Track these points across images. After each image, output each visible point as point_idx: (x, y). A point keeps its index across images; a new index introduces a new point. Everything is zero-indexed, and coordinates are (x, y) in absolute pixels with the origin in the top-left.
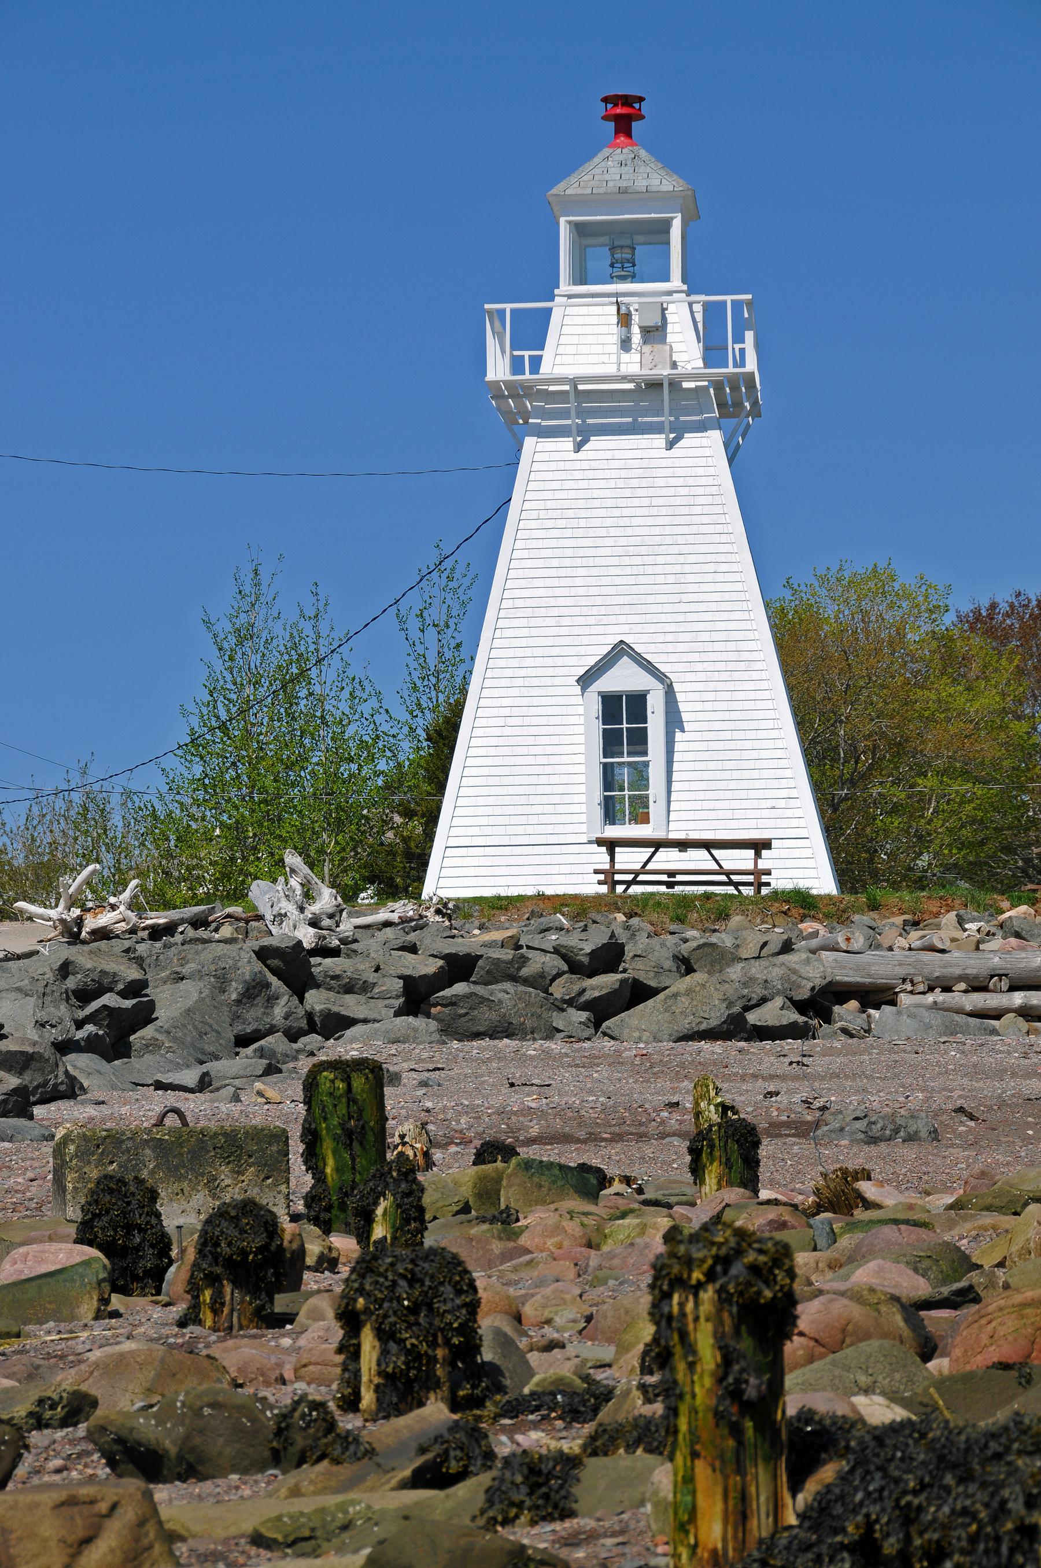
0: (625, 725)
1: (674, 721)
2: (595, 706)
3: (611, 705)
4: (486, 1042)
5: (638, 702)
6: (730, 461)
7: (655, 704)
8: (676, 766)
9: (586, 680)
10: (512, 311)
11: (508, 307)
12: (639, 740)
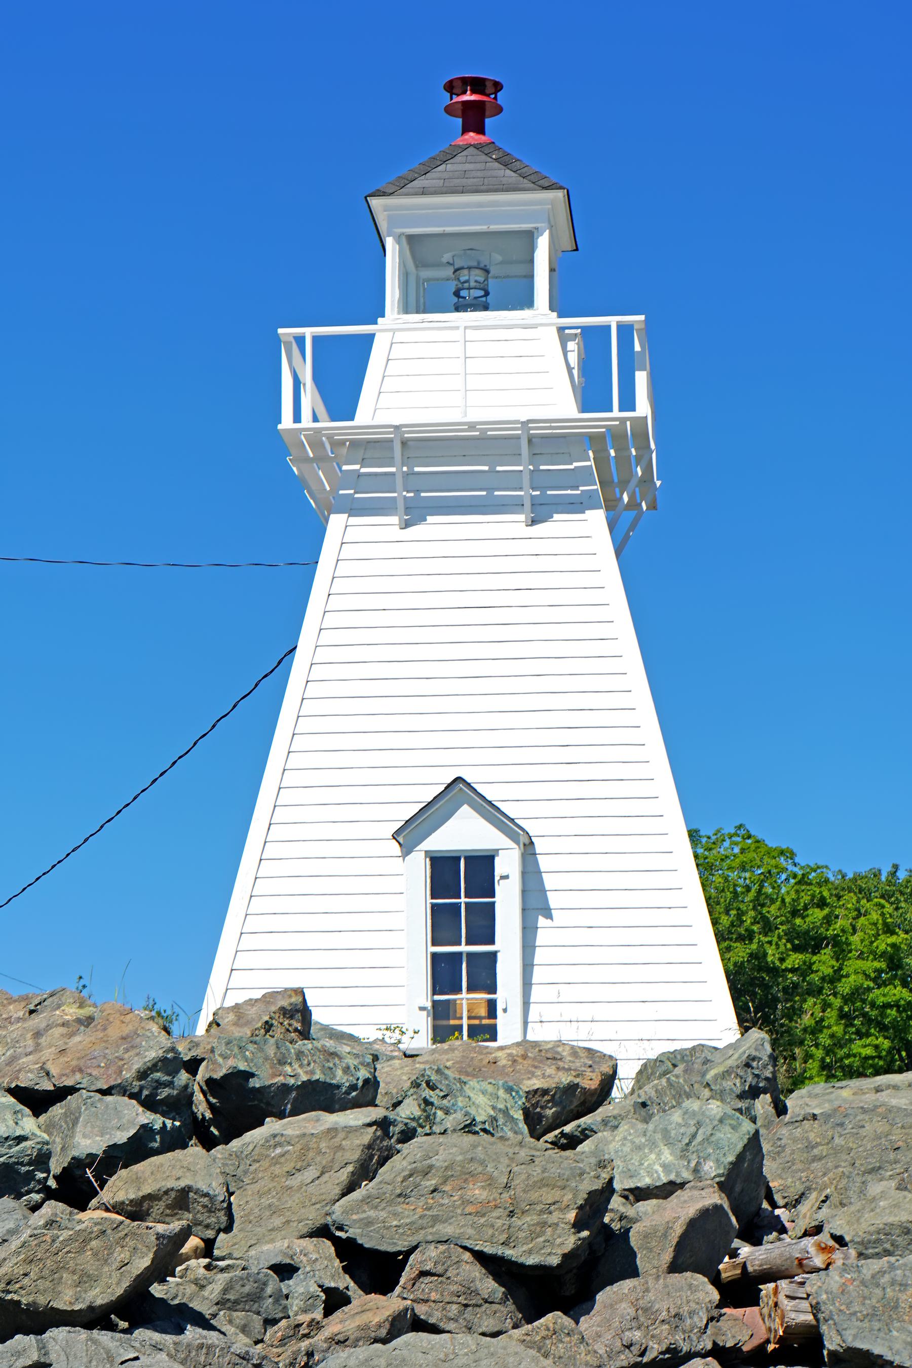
0: (463, 900)
1: (535, 904)
2: (417, 869)
3: (443, 870)
4: (488, 1339)
5: (482, 866)
6: (618, 553)
7: (508, 864)
8: (540, 956)
9: (409, 834)
10: (316, 339)
11: (309, 332)
12: (483, 927)
